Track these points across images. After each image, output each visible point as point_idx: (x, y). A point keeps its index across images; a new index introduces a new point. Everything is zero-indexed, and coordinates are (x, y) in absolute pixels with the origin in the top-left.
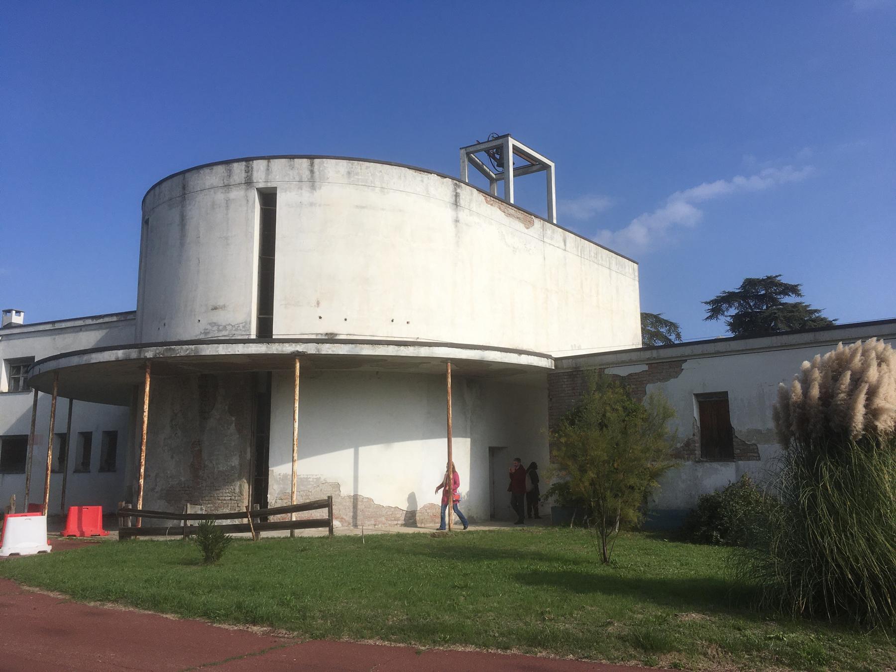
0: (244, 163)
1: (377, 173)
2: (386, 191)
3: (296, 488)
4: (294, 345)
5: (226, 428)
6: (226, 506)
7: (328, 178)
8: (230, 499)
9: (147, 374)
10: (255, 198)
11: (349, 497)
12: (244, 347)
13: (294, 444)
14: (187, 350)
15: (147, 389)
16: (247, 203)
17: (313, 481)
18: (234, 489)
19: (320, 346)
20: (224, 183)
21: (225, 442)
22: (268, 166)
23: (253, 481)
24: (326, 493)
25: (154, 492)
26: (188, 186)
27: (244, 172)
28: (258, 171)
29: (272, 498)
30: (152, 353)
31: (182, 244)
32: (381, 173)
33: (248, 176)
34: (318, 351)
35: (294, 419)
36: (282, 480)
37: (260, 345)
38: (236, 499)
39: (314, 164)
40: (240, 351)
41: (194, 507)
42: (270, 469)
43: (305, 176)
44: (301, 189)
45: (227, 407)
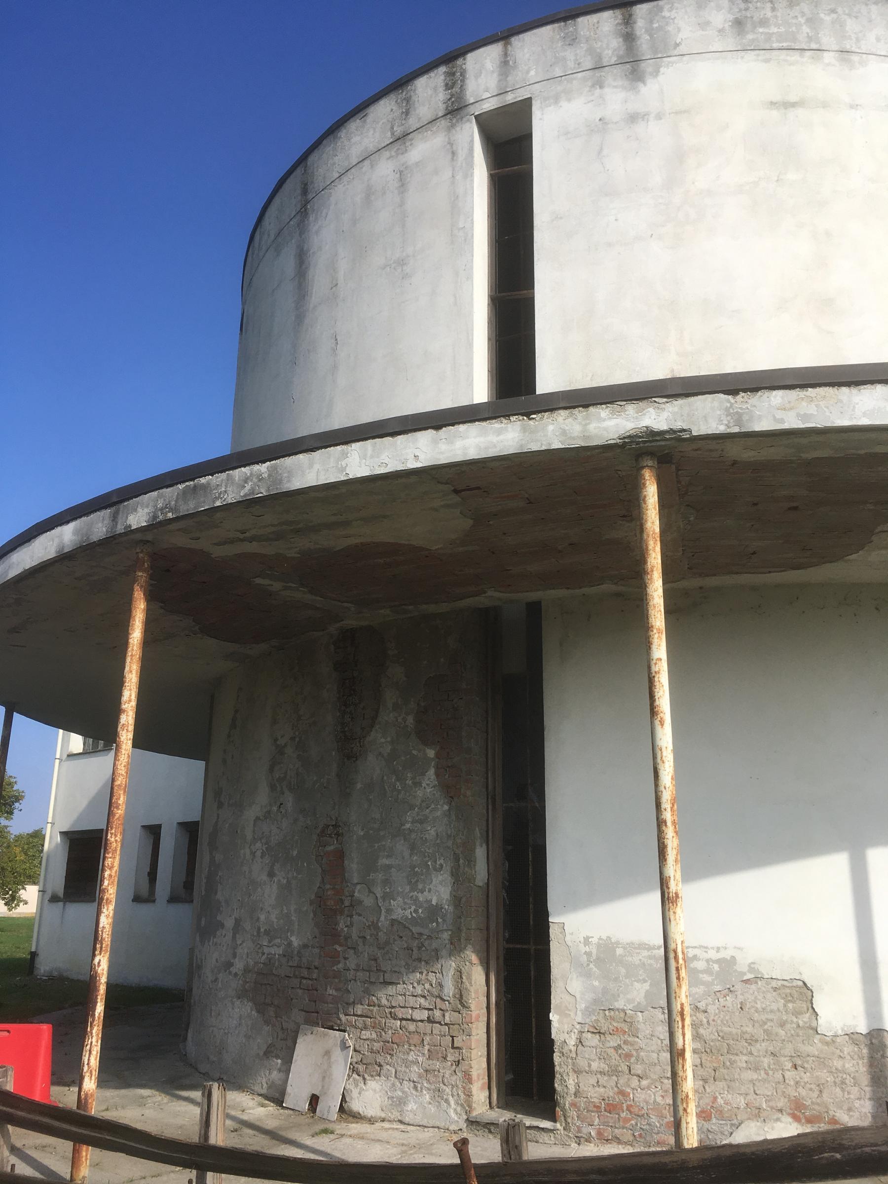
0: (442, 69)
1: (822, 15)
2: (855, 58)
3: (689, 1036)
4: (631, 409)
5: (409, 782)
6: (416, 1039)
7: (677, 45)
8: (430, 1020)
9: (137, 588)
10: (472, 141)
11: (852, 1037)
12: (435, 442)
13: (660, 823)
14: (246, 481)
15: (136, 635)
16: (453, 159)
17: (708, 971)
18: (441, 985)
19: (742, 402)
20: (393, 134)
21: (408, 826)
22: (506, 55)
23: (498, 958)
24: (763, 1017)
25: (230, 973)
26: (312, 182)
27: (441, 89)
28: (477, 76)
29: (566, 1028)
30: (146, 510)
31: (300, 318)
32: (834, 16)
33: (452, 95)
34: (739, 422)
35: (653, 711)
36: (599, 961)
37: (496, 425)
38: (447, 1020)
39: (634, 17)
40: (422, 457)
41: (325, 1035)
42: (550, 920)
43: (610, 52)
44: (601, 87)
45: (410, 720)
